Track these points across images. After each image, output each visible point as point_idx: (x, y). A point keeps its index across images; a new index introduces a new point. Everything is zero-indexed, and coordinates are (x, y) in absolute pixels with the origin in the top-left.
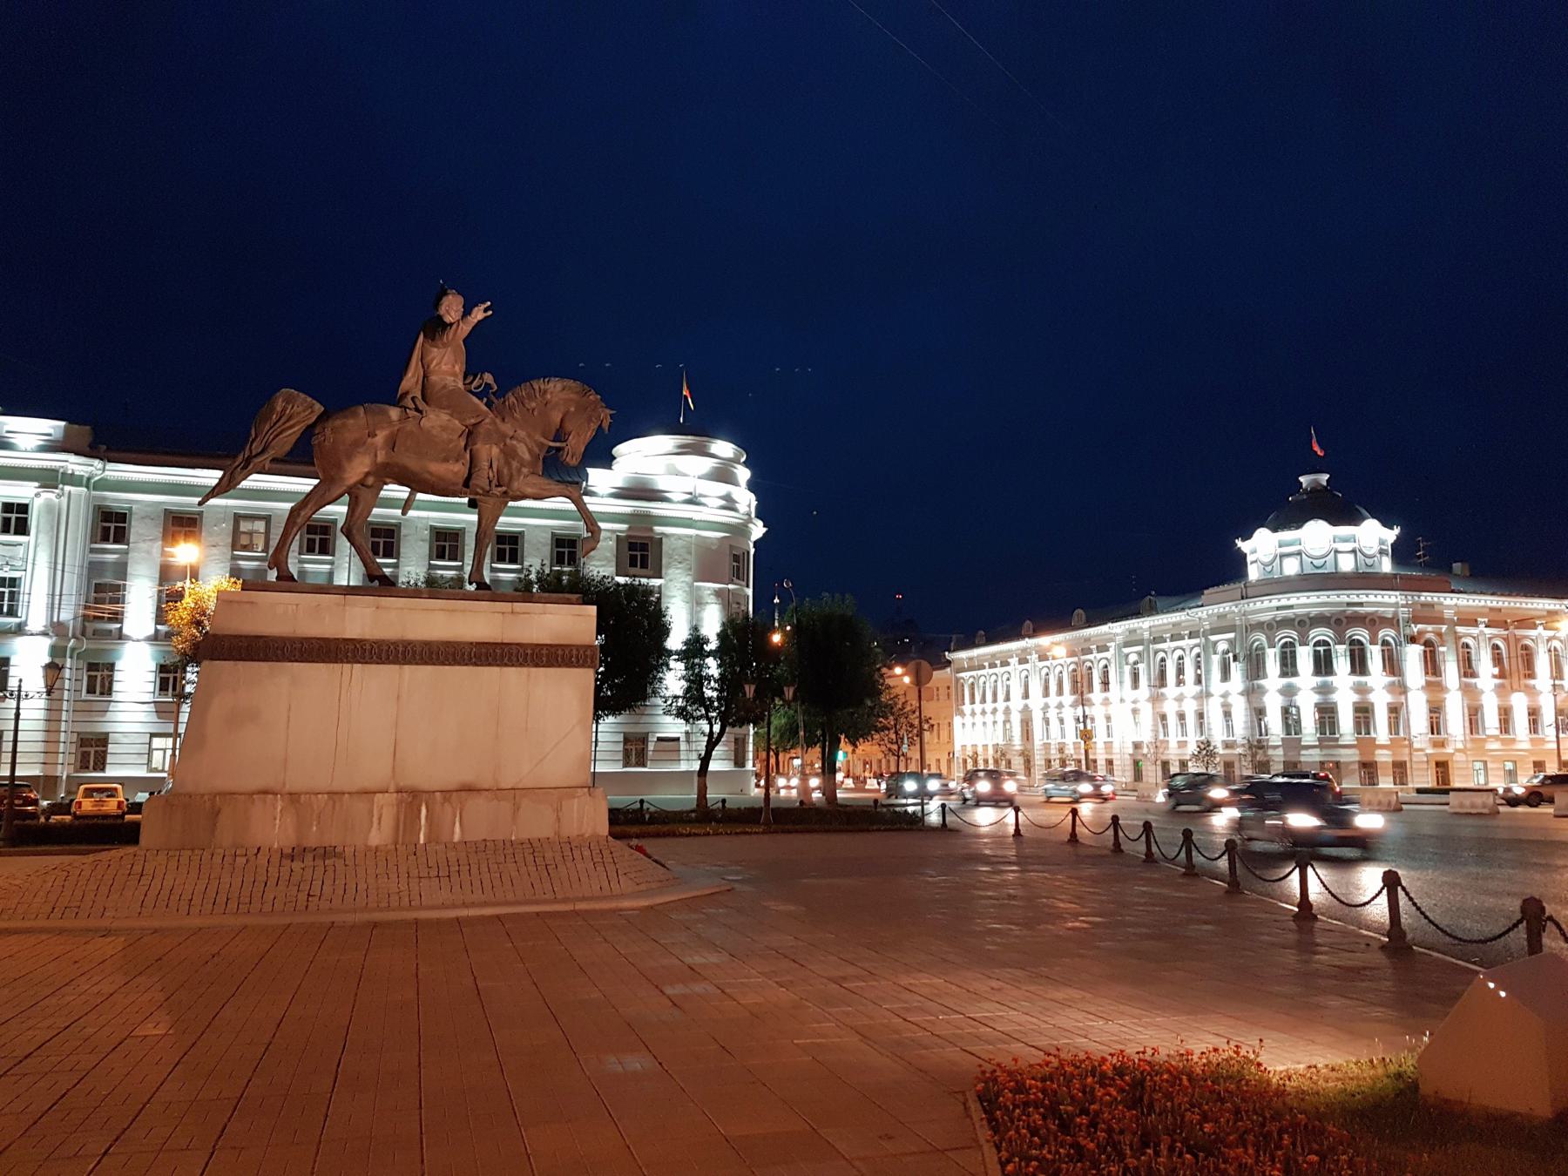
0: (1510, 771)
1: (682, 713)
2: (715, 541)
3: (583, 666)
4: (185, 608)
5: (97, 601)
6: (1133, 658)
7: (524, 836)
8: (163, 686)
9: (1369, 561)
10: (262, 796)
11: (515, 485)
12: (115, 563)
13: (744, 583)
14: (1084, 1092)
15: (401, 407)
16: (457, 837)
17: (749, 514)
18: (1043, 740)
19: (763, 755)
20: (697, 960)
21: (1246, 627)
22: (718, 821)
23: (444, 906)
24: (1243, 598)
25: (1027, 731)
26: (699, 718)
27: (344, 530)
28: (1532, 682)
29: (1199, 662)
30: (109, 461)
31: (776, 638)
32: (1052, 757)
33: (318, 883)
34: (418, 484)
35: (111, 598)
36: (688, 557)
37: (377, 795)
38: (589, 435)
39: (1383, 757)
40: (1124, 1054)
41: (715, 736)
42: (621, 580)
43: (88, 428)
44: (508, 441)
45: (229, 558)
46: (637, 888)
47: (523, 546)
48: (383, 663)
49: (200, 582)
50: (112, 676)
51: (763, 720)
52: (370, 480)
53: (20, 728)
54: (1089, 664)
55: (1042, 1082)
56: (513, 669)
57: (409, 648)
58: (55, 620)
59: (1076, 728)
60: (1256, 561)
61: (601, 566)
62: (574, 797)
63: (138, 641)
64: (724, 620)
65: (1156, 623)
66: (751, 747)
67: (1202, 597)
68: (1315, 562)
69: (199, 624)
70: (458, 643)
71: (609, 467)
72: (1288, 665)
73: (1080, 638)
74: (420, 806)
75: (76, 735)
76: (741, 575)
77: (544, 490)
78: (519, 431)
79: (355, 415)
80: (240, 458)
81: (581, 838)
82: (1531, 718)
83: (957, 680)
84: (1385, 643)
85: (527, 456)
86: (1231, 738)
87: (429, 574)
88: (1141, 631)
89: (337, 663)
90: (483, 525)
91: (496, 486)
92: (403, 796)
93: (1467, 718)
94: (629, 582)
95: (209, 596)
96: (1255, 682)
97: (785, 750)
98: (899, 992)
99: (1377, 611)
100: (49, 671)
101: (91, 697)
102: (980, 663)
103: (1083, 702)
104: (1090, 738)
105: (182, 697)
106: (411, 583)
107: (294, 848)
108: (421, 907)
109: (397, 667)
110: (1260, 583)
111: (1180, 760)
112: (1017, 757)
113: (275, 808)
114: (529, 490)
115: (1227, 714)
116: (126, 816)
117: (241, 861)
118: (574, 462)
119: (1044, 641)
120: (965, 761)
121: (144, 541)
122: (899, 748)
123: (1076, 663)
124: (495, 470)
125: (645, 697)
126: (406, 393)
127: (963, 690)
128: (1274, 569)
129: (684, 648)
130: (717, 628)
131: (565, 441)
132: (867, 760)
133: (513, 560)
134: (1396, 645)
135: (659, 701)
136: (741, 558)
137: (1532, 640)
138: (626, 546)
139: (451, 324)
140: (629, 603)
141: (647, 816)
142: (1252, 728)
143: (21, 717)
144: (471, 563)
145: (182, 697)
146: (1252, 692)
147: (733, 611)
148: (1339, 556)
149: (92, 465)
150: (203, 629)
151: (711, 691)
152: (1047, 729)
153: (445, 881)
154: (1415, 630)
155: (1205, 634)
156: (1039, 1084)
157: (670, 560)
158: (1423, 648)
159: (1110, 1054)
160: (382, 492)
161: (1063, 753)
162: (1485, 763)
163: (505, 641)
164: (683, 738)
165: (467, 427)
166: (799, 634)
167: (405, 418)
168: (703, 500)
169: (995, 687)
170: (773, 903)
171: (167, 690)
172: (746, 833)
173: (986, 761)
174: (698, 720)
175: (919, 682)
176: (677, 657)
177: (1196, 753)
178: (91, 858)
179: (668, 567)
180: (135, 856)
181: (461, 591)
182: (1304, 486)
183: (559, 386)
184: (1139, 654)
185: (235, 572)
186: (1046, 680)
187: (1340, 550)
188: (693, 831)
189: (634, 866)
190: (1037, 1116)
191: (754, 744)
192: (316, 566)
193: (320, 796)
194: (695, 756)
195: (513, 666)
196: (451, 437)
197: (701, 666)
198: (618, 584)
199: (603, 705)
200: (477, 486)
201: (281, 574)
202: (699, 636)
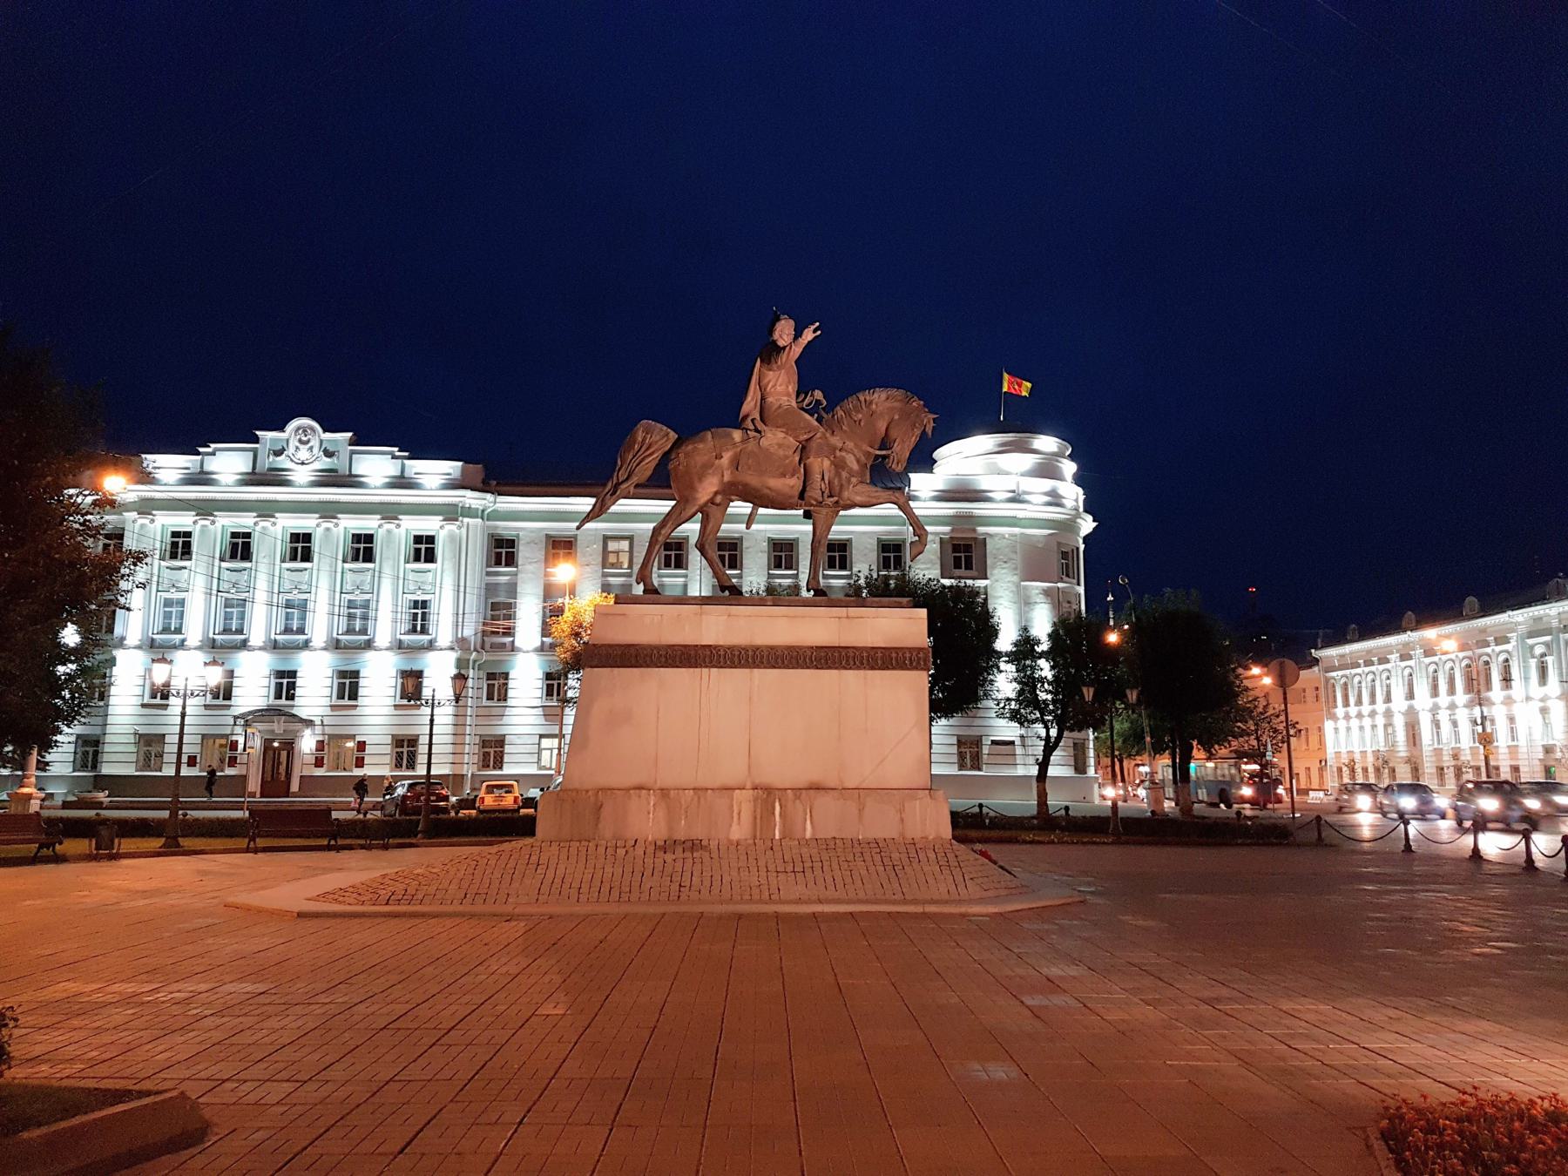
1: (1015, 717)
2: (1041, 539)
3: (916, 668)
4: (566, 622)
5: (493, 618)
6: (1539, 650)
8: (549, 693)
10: (637, 791)
11: (846, 494)
12: (505, 583)
13: (1075, 581)
14: (1511, 1139)
15: (742, 429)
16: (808, 835)
17: (1076, 509)
18: (1433, 744)
19: (1108, 761)
20: (1054, 971)
22: (1062, 829)
23: (799, 901)
25: (1414, 734)
26: (1034, 722)
27: (698, 546)
30: (499, 495)
31: (1113, 638)
32: (1445, 765)
33: (687, 875)
34: (758, 499)
35: (504, 615)
36: (1014, 556)
37: (737, 791)
38: (913, 440)
40: (1558, 1097)
41: (1053, 740)
42: (947, 582)
43: (481, 466)
44: (838, 453)
45: (600, 574)
46: (985, 894)
47: (851, 553)
48: (736, 667)
49: (578, 598)
50: (507, 684)
51: (1104, 725)
52: (719, 499)
53: (434, 732)
54: (1486, 658)
55: (1458, 1122)
56: (851, 672)
57: (757, 653)
58: (460, 636)
59: (1473, 730)
61: (926, 569)
63: (528, 652)
64: (1055, 620)
66: (1091, 753)
69: (577, 635)
70: (800, 648)
71: (931, 471)
73: (1474, 629)
74: (774, 802)
75: (478, 737)
76: (1071, 574)
77: (872, 497)
78: (847, 443)
79: (703, 440)
80: (609, 485)
81: (924, 840)
83: (1327, 680)
85: (855, 466)
87: (769, 583)
89: (697, 667)
90: (818, 533)
91: (828, 497)
92: (758, 793)
94: (954, 584)
95: (586, 610)
97: (1129, 756)
98: (1281, 1018)
100: (457, 681)
101: (490, 703)
102: (1354, 661)
104: (1490, 742)
105: (566, 701)
106: (753, 592)
108: (781, 902)
109: (747, 670)
112: (1402, 765)
113: (649, 804)
114: (858, 499)
116: (522, 810)
117: (621, 852)
118: (899, 469)
119: (1430, 633)
120: (1340, 770)
121: (530, 563)
123: (1470, 658)
124: (827, 482)
125: (977, 699)
126: (746, 417)
127: (1334, 691)
129: (1014, 649)
130: (1049, 629)
131: (890, 448)
133: (843, 567)
135: (991, 704)
138: (950, 549)
139: (784, 348)
140: (956, 604)
141: (987, 821)
143: (435, 723)
144: (808, 571)
145: (566, 701)
147: (1064, 610)
149: (485, 499)
150: (581, 639)
151: (1045, 693)
152: (1438, 733)
156: (1454, 1124)
159: (1540, 1097)
160: (729, 509)
161: (1458, 759)
165: (800, 443)
166: (1137, 634)
167: (745, 440)
168: (1027, 497)
169: (1373, 687)
170: (1130, 918)
171: (552, 695)
172: (1095, 843)
173: (1365, 770)
174: (1033, 723)
175: (1283, 682)
176: (1007, 659)
178: (494, 849)
179: (993, 568)
180: (532, 847)
181: (797, 598)
183: (884, 396)
185: (606, 588)
186: (1434, 678)
189: (980, 871)
190: (1455, 1161)
191: (1095, 750)
192: (669, 580)
194: (1032, 760)
195: (851, 669)
197: (1033, 668)
198: (944, 587)
199: (939, 708)
200: (810, 497)
201: (647, 588)
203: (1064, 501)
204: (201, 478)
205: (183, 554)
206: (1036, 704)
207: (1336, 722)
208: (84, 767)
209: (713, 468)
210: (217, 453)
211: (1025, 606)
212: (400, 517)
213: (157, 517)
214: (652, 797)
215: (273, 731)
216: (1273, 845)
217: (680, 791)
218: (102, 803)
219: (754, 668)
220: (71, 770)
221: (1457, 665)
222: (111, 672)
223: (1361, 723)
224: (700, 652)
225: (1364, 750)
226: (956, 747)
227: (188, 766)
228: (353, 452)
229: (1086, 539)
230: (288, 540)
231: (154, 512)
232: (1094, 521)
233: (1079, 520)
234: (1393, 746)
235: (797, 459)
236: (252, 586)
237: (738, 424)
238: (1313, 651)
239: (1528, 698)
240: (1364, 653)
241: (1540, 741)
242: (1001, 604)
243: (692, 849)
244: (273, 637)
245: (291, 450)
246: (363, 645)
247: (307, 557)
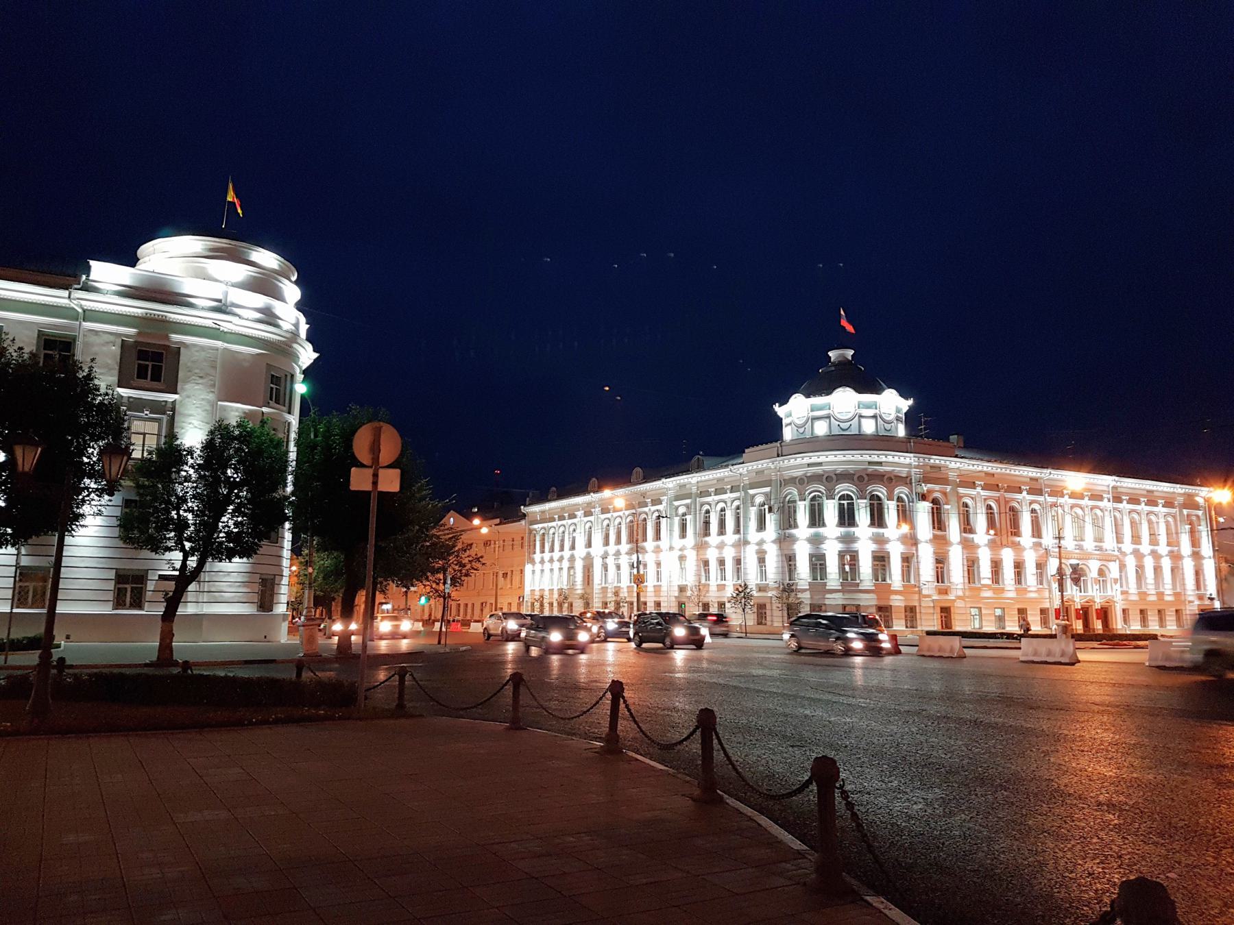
0: (999, 616)
6: (682, 510)
9: (888, 426)
13: (285, 409)
18: (601, 584)
21: (780, 481)
24: (778, 456)
28: (1018, 539)
29: (738, 513)
36: (212, 371)
39: (897, 602)
59: (631, 573)
60: (790, 424)
65: (703, 478)
67: (744, 455)
68: (842, 425)
72: (816, 518)
76: (281, 401)
82: (1016, 570)
83: (531, 531)
84: (900, 499)
86: (764, 582)
88: (690, 485)
93: (966, 569)
96: (787, 531)
99: (894, 470)
102: (551, 516)
103: (638, 550)
104: (642, 582)
110: (794, 442)
111: (718, 602)
115: (762, 561)
119: (607, 493)
120: (533, 604)
127: (535, 541)
128: (806, 430)
134: (909, 502)
136: (283, 380)
137: (1018, 502)
138: (134, 355)
142: (783, 573)
146: (785, 540)
148: (863, 420)
152: (605, 574)
154: (925, 489)
155: (745, 489)
158: (931, 505)
162: (980, 609)
173: (551, 604)
177: (735, 595)
179: (186, 381)
182: (832, 360)
184: (688, 506)
187: (863, 415)
221: (624, 520)
223: (542, 567)
225: (552, 588)
233: (295, 346)
234: (573, 585)
238: (522, 507)
239: (671, 548)
240: (559, 510)
241: (677, 582)
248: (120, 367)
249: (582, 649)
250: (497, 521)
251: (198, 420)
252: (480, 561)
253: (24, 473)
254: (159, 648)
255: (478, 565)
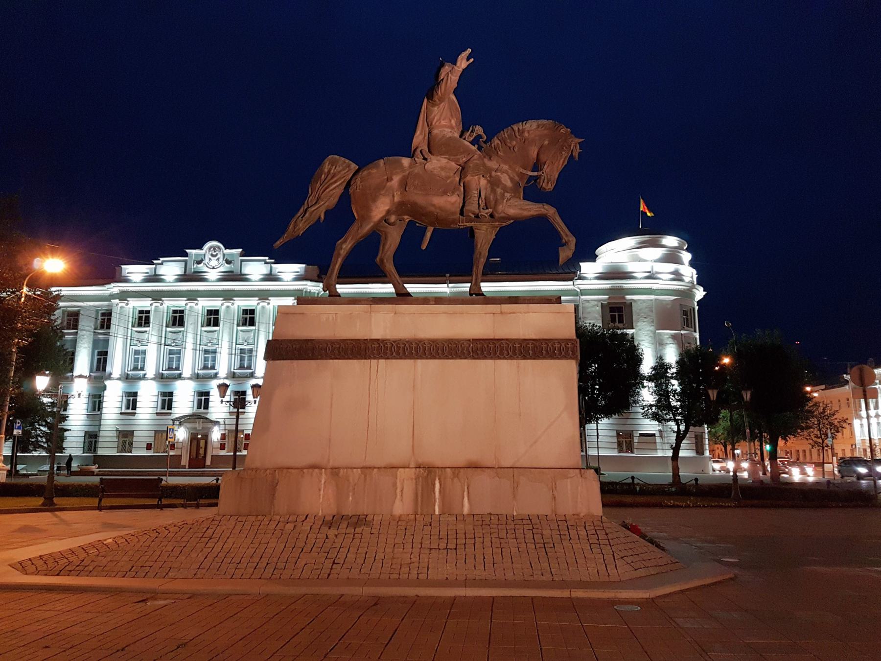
7: (526, 511)
10: (311, 470)
11: (500, 208)
13: (693, 330)
16: (466, 510)
17: (692, 283)
22: (695, 495)
26: (670, 420)
33: (344, 551)
37: (400, 469)
43: (316, 267)
44: (493, 173)
56: (505, 361)
62: (568, 478)
70: (459, 340)
71: (595, 261)
74: (435, 480)
76: (690, 325)
81: (576, 517)
85: (509, 184)
89: (366, 359)
92: (420, 471)
107: (334, 516)
122: (823, 441)
131: (541, 170)
132: (788, 450)
138: (608, 310)
149: (319, 286)
153: (452, 554)
157: (639, 317)
163: (496, 338)
164: (657, 434)
165: (460, 165)
166: (736, 357)
168: (659, 276)
172: (722, 507)
188: (676, 503)
193: (355, 470)
194: (667, 446)
196: (448, 174)
197: (667, 385)
202: (664, 363)
203: (684, 277)
204: (154, 278)
205: (145, 323)
206: (670, 408)
207: (861, 420)
208: (89, 450)
209: (385, 189)
210: (164, 263)
211: (659, 346)
212: (270, 298)
213: (130, 302)
214: (324, 475)
215: (195, 428)
216: (861, 507)
217: (349, 470)
218: (93, 472)
219: (418, 359)
220: (82, 452)
222: (104, 393)
224: (369, 345)
226: (616, 437)
227: (147, 450)
228: (242, 261)
229: (699, 303)
230: (206, 314)
231: (128, 299)
232: (704, 291)
233: (694, 290)
235: (457, 179)
236: (184, 341)
237: (409, 153)
238: (845, 375)
242: (643, 345)
243: (356, 525)
244: (196, 371)
245: (207, 260)
246: (249, 375)
247: (216, 324)
248: (602, 318)
249: (159, 501)
250: (823, 387)
251: (648, 343)
252: (846, 422)
253: (713, 401)
254: (48, 479)
255: (844, 425)
